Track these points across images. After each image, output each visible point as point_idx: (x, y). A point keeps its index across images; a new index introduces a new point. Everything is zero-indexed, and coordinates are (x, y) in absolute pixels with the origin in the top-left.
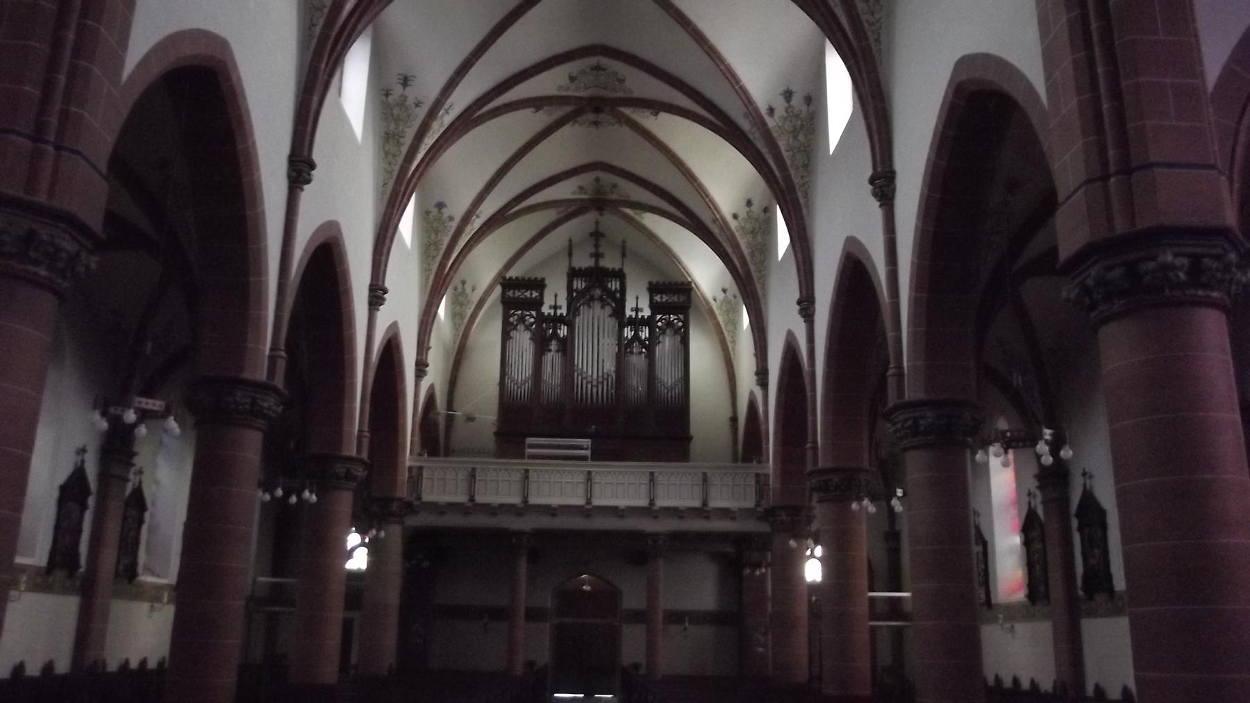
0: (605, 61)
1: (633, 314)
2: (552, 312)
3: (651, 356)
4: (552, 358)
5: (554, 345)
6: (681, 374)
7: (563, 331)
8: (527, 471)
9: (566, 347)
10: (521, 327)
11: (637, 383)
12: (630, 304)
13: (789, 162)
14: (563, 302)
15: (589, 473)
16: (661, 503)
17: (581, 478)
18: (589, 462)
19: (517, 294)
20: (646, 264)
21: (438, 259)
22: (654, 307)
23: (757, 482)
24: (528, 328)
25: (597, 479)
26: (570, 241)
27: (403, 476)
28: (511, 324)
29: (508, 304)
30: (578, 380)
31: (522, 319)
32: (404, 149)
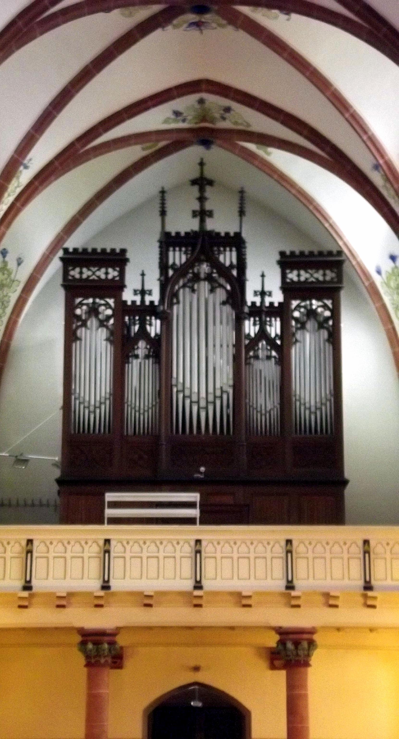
3: (284, 362)
4: (139, 371)
5: (142, 348)
7: (155, 327)
8: (107, 541)
9: (159, 350)
10: (93, 322)
11: (264, 402)
12: (252, 285)
18: (198, 527)
19: (86, 273)
20: (278, 219)
22: (289, 290)
24: (102, 324)
28: (79, 318)
29: (74, 289)
31: (93, 311)
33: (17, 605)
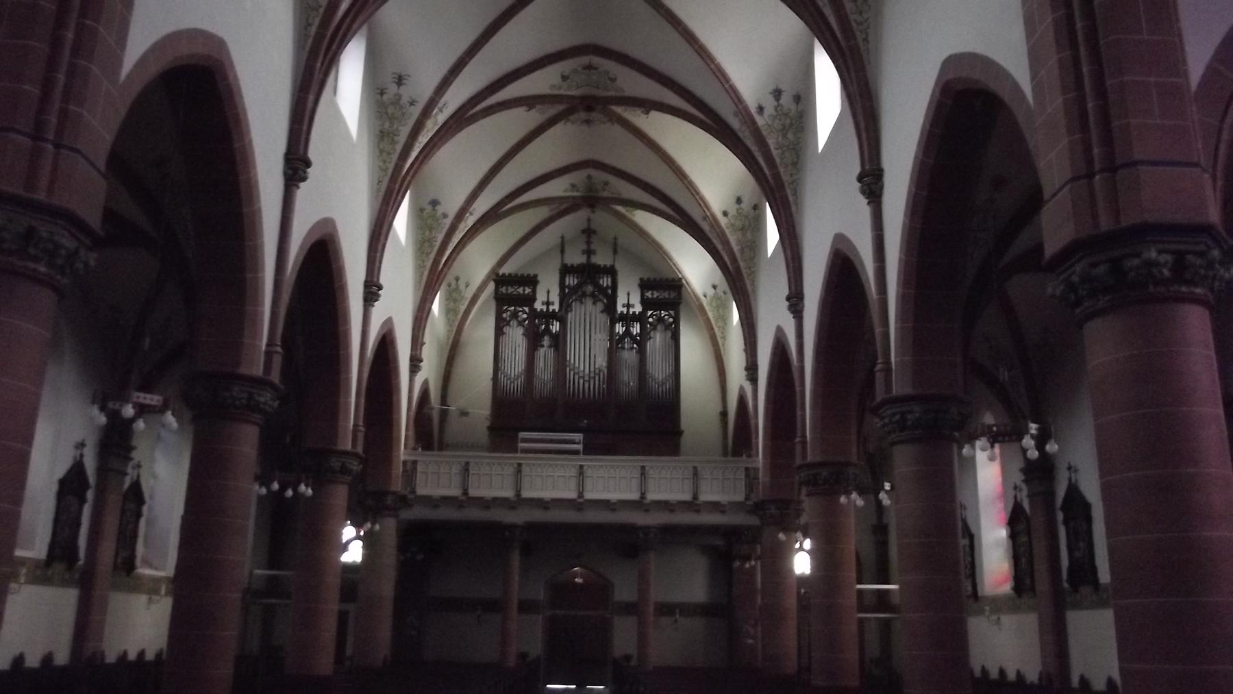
0: (596, 60)
1: (625, 310)
2: (545, 308)
3: (642, 351)
4: (545, 354)
5: (546, 341)
6: (671, 369)
7: (555, 327)
8: (520, 465)
9: (559, 342)
10: (514, 323)
11: (628, 378)
12: (621, 300)
13: (778, 160)
14: (555, 298)
15: (581, 467)
16: (652, 496)
17: (573, 472)
18: (581, 456)
19: (510, 290)
20: (638, 261)
21: (432, 256)
22: (645, 303)
23: (747, 476)
24: (521, 323)
25: (588, 472)
26: (562, 238)
27: (398, 470)
28: (504, 320)
29: (502, 300)
30: (570, 375)
31: (515, 315)
32: (399, 148)
33: (783, 87)
